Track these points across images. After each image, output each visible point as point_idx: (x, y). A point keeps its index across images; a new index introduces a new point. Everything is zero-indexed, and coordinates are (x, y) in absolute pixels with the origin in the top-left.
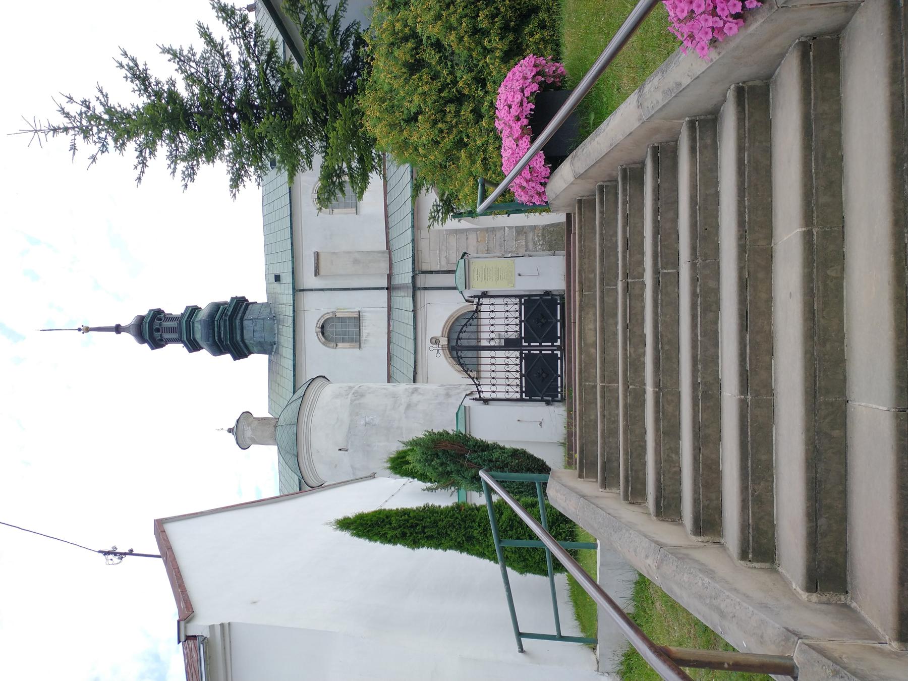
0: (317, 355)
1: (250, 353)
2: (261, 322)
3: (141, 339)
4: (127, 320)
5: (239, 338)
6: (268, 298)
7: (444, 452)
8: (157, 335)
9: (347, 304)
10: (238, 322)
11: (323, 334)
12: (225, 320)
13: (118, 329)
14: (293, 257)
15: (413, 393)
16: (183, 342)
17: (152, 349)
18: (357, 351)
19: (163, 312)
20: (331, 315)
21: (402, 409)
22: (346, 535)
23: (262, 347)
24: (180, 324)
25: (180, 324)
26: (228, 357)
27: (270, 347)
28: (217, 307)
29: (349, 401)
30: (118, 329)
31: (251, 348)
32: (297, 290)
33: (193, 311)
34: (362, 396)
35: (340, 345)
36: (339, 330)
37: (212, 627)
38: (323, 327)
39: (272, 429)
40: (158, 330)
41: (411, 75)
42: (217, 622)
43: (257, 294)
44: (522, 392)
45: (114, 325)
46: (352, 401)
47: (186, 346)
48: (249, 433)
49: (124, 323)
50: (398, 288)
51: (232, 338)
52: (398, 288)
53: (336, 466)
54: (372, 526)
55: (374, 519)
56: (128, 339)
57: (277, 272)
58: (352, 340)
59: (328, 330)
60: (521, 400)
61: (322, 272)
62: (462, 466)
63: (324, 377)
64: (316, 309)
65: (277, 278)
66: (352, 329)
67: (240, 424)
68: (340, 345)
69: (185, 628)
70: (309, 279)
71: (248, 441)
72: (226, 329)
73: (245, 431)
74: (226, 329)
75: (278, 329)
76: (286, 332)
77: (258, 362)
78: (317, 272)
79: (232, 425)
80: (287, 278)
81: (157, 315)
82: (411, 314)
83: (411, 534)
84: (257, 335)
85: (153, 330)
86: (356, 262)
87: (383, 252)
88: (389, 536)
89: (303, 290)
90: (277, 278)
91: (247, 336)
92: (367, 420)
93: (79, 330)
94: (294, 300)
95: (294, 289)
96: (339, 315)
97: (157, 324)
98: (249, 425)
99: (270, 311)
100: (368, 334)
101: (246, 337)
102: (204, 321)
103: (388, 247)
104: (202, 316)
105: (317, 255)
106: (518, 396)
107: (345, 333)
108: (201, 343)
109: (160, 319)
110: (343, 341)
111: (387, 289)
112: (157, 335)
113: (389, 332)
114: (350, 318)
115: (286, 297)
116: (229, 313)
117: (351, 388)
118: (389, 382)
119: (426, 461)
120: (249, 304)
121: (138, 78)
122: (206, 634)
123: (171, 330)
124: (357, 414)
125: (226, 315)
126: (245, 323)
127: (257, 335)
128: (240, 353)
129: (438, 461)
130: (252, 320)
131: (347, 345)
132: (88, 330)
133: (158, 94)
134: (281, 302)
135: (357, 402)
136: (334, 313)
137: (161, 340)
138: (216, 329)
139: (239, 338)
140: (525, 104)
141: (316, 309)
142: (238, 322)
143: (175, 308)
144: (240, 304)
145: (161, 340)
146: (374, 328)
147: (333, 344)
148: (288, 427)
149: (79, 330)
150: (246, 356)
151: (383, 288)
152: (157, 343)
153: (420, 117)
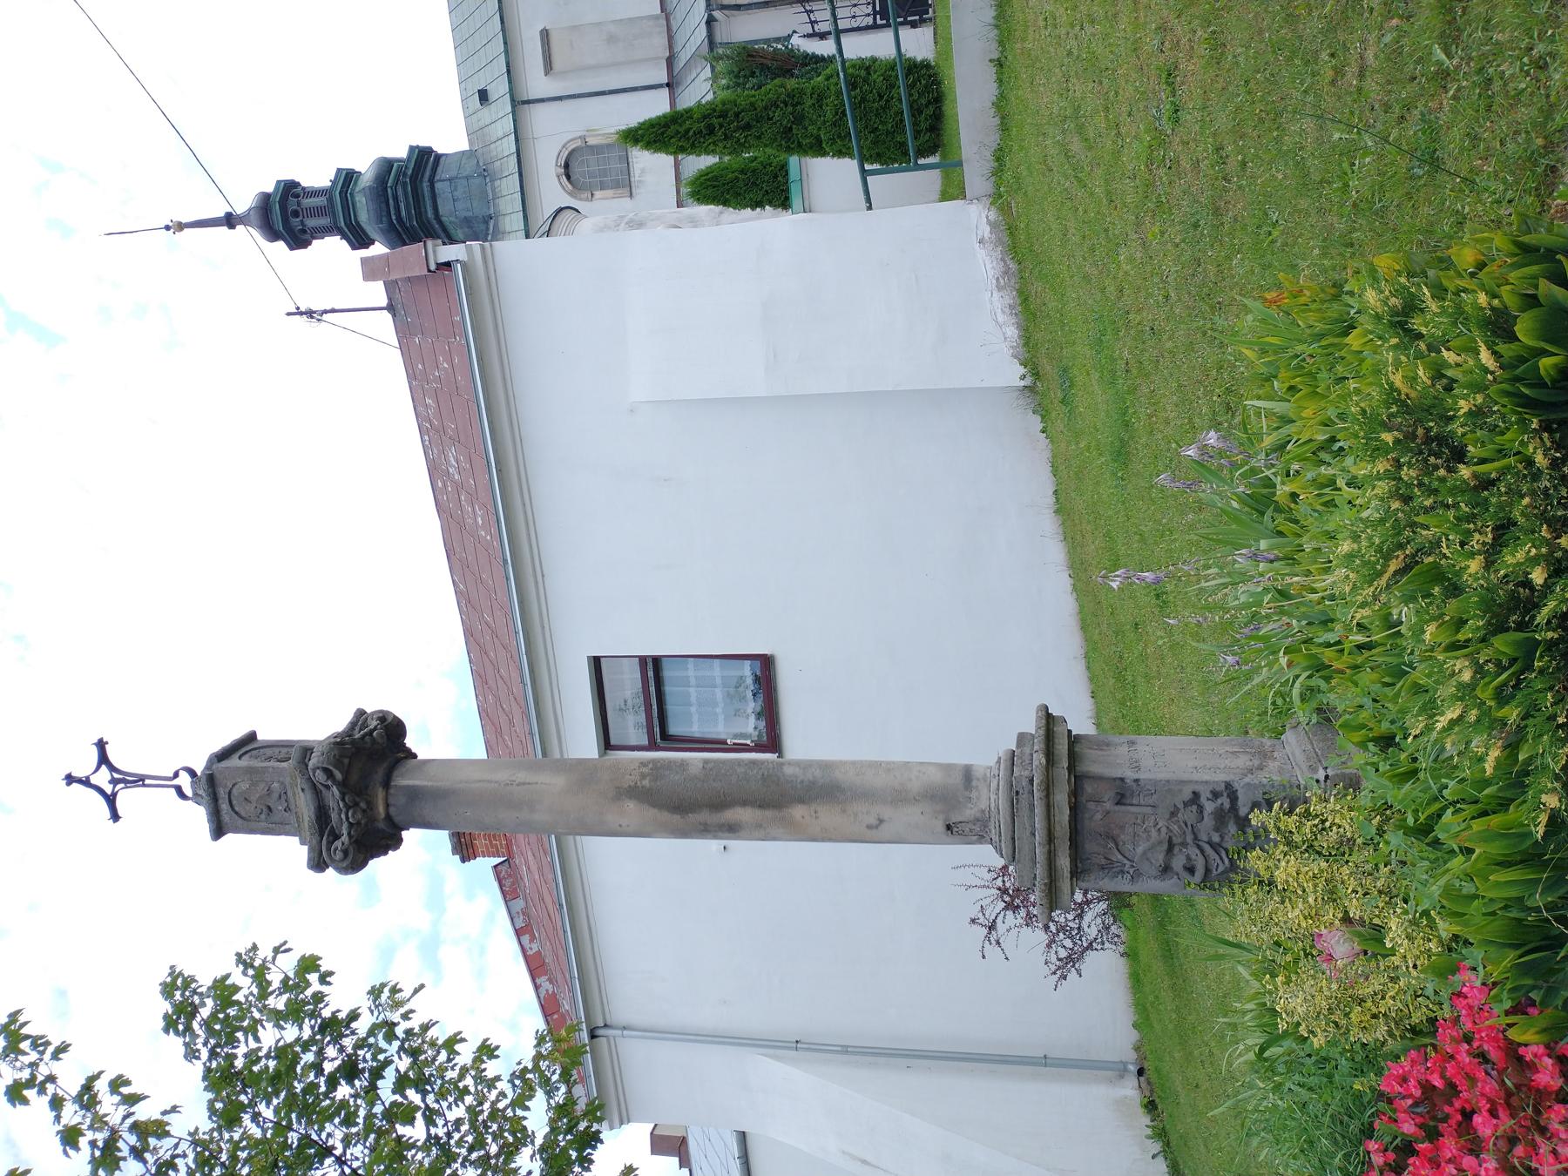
2: (464, 182)
3: (272, 234)
4: (243, 202)
5: (430, 214)
6: (471, 142)
8: (295, 221)
10: (425, 184)
11: (568, 177)
13: (230, 221)
17: (292, 248)
19: (298, 184)
20: (579, 143)
24: (331, 200)
25: (331, 200)
27: (483, 227)
28: (387, 165)
30: (230, 221)
32: (519, 103)
33: (347, 178)
35: (598, 194)
38: (567, 166)
40: (296, 214)
43: (450, 138)
44: (875, 13)
47: (344, 237)
49: (241, 207)
51: (420, 214)
56: (247, 238)
58: (617, 185)
59: (576, 170)
60: (875, 27)
61: (558, 62)
65: (483, 96)
66: (617, 165)
68: (598, 194)
70: (536, 83)
75: (493, 190)
76: (509, 186)
78: (548, 66)
80: (499, 89)
81: (289, 189)
83: (721, 126)
84: (460, 205)
87: (656, 17)
89: (529, 102)
90: (483, 96)
91: (444, 209)
93: (167, 228)
95: (513, 100)
96: (592, 141)
97: (292, 204)
99: (478, 167)
100: (643, 171)
101: (441, 212)
104: (367, 179)
105: (545, 35)
106: (870, 20)
107: (604, 173)
108: (373, 234)
111: (668, 85)
112: (295, 221)
117: (622, 217)
120: (438, 157)
123: (318, 212)
125: (405, 175)
126: (438, 186)
127: (460, 205)
128: (393, 842)
131: (609, 193)
132: (181, 226)
136: (583, 138)
137: (304, 231)
139: (430, 214)
142: (425, 184)
143: (317, 177)
144: (424, 158)
145: (304, 231)
147: (588, 194)
149: (167, 228)
151: (660, 86)
152: (298, 240)
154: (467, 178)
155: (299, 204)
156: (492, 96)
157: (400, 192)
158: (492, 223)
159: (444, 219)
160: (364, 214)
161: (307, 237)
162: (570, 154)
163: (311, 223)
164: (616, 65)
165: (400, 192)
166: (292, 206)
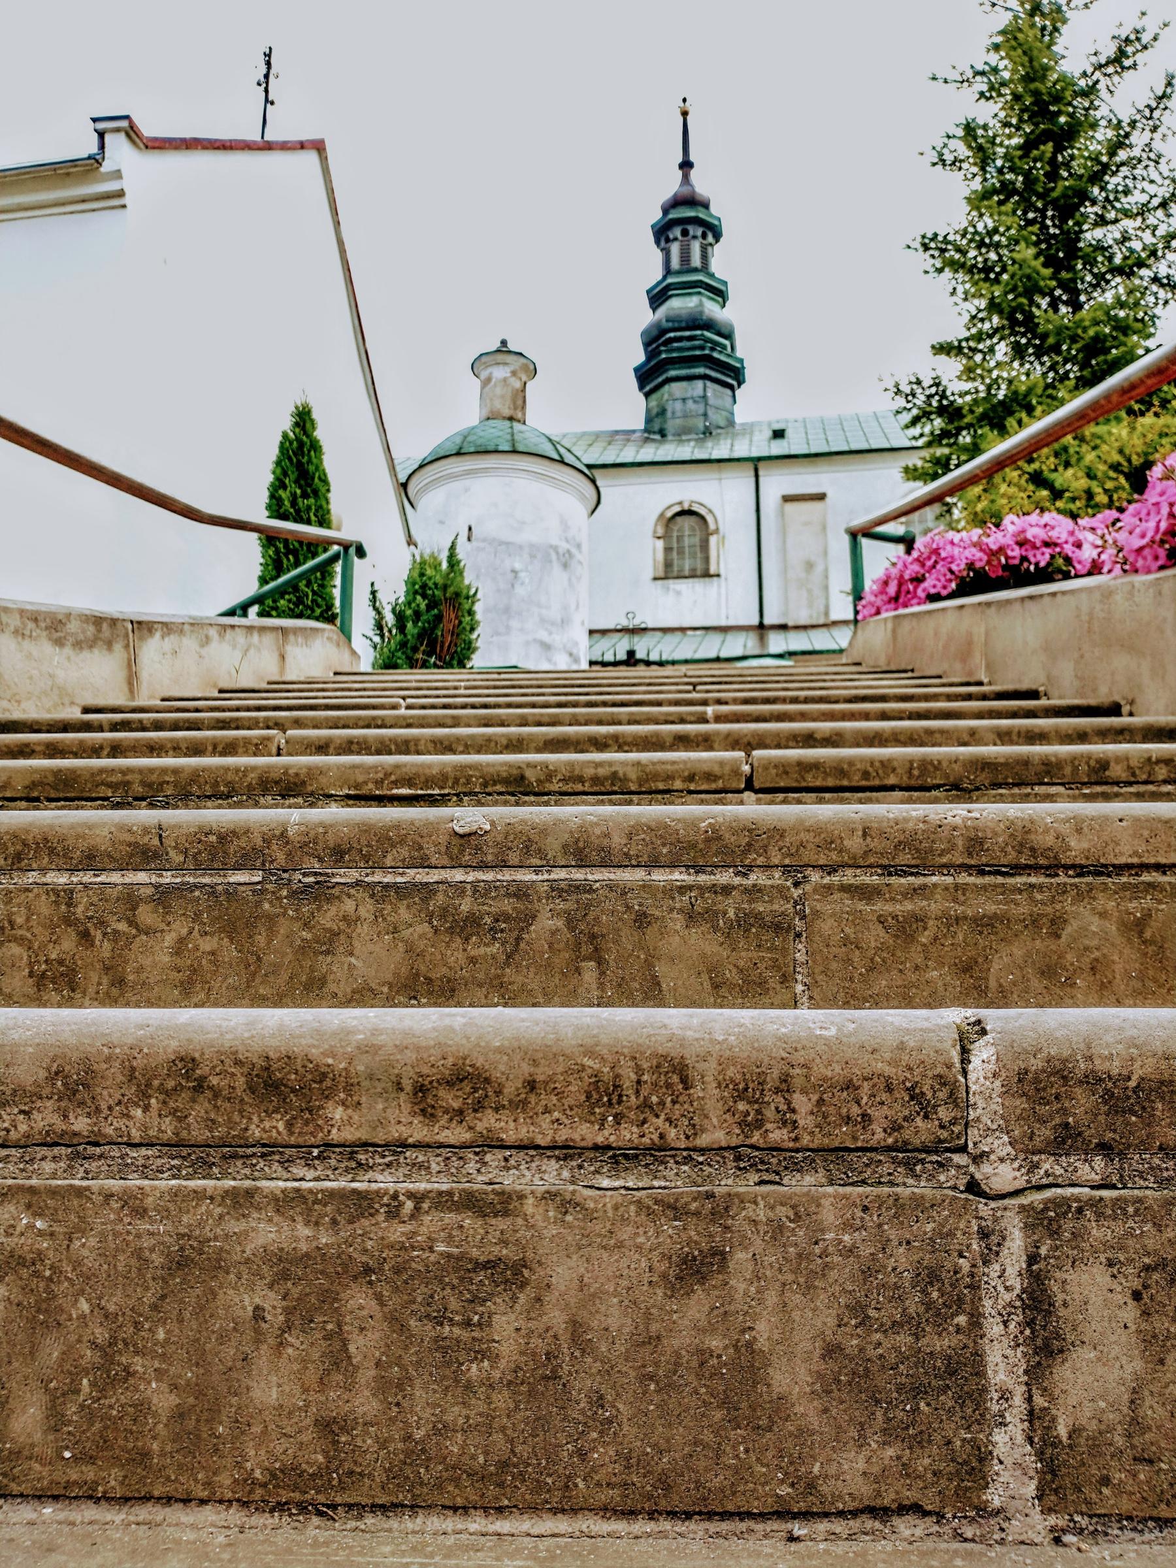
0: (643, 501)
1: (647, 395)
2: (701, 411)
4: (701, 185)
7: (439, 618)
8: (677, 232)
9: (732, 552)
10: (701, 370)
11: (682, 513)
12: (702, 348)
13: (686, 165)
14: (817, 455)
15: (571, 655)
16: (665, 278)
18: (650, 574)
20: (712, 526)
21: (543, 635)
22: (286, 423)
23: (658, 415)
24: (696, 270)
25: (696, 270)
26: (640, 357)
27: (656, 428)
29: (555, 541)
30: (686, 165)
31: (654, 396)
32: (756, 463)
34: (565, 566)
35: (660, 544)
36: (686, 543)
37: (117, 175)
39: (507, 412)
40: (685, 233)
41: (1128, 477)
42: (125, 184)
43: (753, 406)
45: (692, 158)
46: (555, 548)
48: (499, 373)
50: (762, 640)
52: (762, 640)
53: (442, 522)
54: (300, 465)
55: (311, 468)
56: (671, 185)
57: (788, 433)
58: (668, 565)
59: (687, 523)
61: (790, 507)
62: (415, 649)
63: (599, 502)
64: (724, 498)
65: (779, 434)
66: (687, 566)
67: (515, 357)
68: (660, 544)
69: (118, 130)
70: (776, 484)
71: (484, 375)
72: (685, 354)
73: (506, 365)
74: (685, 354)
77: (632, 409)
78: (787, 499)
79: (512, 346)
82: (713, 655)
85: (686, 221)
86: (810, 566)
87: (827, 614)
88: (281, 492)
90: (779, 434)
91: (677, 388)
92: (522, 575)
94: (738, 460)
95: (760, 459)
96: (713, 540)
98: (514, 373)
102: (701, 313)
103: (835, 623)
105: (821, 497)
107: (681, 552)
108: (662, 311)
109: (704, 236)
110: (668, 550)
112: (677, 232)
113: (683, 630)
114: (707, 559)
115: (742, 449)
116: (715, 355)
117: (579, 546)
118: (591, 632)
119: (424, 586)
121: (1121, 54)
122: (107, 167)
123: (685, 257)
124: (533, 556)
125: (712, 349)
126: (699, 384)
127: (678, 406)
128: (649, 377)
129: (423, 606)
130: (704, 397)
131: (660, 556)
132: (685, 114)
133: (1090, 92)
134: (736, 443)
135: (554, 556)
136: (717, 531)
137: (668, 240)
138: (687, 333)
139: (673, 373)
140: (1048, 551)
141: (724, 498)
142: (701, 370)
144: (731, 375)
146: (688, 603)
147: (660, 532)
148: (509, 437)
150: (641, 388)
152: (662, 233)
153: (1045, 493)
154: (705, 415)
155: (695, 237)
156: (778, 442)
157: (697, 343)
158: (657, 437)
159: (666, 387)
160: (679, 305)
161: (663, 243)
162: (703, 518)
163: (675, 248)
164: (785, 570)
165: (697, 343)
166: (692, 230)
